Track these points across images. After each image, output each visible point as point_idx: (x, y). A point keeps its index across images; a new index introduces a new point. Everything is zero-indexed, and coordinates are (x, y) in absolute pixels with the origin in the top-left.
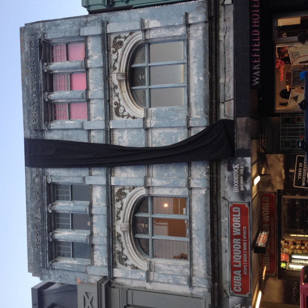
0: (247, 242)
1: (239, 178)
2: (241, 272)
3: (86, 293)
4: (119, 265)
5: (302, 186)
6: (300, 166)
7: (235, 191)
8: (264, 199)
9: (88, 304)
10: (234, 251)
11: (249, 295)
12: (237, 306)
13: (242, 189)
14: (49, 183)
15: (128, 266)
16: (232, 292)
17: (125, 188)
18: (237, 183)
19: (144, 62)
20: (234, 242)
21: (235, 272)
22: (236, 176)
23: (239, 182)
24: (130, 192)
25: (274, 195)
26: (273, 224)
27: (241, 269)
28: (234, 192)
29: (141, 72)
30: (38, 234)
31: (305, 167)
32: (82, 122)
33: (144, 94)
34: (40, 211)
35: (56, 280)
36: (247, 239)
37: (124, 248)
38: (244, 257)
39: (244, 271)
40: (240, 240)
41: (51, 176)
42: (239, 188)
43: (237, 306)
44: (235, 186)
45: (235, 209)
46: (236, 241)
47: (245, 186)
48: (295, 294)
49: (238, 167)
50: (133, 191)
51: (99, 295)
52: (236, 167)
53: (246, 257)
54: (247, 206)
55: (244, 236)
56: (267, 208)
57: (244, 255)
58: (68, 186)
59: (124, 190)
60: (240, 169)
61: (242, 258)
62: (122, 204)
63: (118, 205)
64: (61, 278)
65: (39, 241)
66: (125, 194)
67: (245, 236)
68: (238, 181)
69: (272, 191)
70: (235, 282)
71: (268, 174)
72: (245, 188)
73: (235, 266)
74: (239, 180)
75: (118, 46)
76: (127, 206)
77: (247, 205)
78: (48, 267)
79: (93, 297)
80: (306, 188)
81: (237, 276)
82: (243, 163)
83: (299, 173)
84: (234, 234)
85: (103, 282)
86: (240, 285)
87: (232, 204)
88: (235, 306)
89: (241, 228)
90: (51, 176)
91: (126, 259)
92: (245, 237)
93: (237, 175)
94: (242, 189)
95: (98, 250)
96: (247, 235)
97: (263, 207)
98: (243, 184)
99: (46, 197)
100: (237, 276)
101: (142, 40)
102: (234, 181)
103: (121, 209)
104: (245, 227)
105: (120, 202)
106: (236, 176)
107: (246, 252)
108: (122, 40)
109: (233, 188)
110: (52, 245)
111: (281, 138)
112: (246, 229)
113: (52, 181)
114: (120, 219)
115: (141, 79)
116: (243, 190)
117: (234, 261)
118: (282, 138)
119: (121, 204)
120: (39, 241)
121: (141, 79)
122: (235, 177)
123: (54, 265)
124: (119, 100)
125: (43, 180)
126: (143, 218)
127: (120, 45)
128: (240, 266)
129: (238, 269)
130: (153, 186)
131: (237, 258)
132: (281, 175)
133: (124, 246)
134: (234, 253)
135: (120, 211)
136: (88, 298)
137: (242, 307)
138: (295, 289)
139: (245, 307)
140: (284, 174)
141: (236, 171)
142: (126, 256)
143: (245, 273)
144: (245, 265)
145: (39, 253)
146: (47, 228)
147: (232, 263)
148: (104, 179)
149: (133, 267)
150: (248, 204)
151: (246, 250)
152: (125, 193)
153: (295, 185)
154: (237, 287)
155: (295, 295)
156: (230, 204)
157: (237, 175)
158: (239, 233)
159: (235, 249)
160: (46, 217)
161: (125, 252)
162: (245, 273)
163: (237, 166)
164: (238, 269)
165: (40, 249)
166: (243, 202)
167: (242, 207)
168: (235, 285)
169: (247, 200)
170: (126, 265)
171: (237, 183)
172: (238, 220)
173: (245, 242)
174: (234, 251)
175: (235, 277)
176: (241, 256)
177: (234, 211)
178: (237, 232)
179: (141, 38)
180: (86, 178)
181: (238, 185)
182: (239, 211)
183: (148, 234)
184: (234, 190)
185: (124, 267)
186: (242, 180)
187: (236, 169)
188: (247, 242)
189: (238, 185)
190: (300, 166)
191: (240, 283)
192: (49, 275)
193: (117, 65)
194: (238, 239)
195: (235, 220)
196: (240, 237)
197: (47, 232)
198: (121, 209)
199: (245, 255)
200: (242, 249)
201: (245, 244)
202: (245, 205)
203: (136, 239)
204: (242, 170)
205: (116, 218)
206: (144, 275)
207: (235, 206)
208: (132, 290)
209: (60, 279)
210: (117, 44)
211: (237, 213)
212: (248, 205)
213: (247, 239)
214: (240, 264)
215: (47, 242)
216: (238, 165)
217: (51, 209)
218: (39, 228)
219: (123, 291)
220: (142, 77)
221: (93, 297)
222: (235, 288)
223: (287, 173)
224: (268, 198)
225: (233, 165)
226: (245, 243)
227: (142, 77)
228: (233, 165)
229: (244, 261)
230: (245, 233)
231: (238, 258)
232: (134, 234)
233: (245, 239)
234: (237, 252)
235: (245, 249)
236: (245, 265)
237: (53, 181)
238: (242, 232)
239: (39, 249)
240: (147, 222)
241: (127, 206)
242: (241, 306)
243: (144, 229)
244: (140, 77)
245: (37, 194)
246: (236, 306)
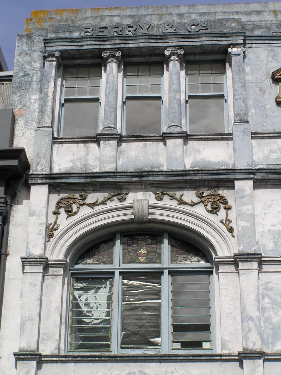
4: (55, 198)
14: (230, 50)
15: (55, 216)
17: (229, 211)
24: (222, 222)
30: (118, 27)
32: (248, 122)
34: (167, 31)
35: (19, 66)
37: (93, 209)
41: (244, 53)
50: (223, 229)
58: (222, 90)
59: (225, 208)
62: (193, 204)
63: (190, 196)
64: (24, 76)
65: (101, 30)
66: (215, 210)
76: (189, 215)
78: (47, 49)
90: (244, 53)
91: (69, 212)
95: (88, 153)
99: (198, 43)
103: (181, 202)
105: (196, 200)
110: (93, 57)
113: (234, 55)
114: (158, 200)
119: (192, 202)
120: (101, 30)
123: (52, 61)
125: (235, 38)
126: (158, 251)
130: (238, 273)
133: (98, 209)
135: (175, 199)
142: (76, 213)
145: (77, 31)
146: (131, 45)
148: (246, 164)
149: (53, 227)
152: (218, 211)
160: (155, 45)
161: (85, 211)
165: (86, 32)
170: (56, 213)
179: (220, 254)
180: (246, 126)
183: (123, 263)
185: (53, 207)
192: (29, 52)
193: (167, 202)
197: (122, 46)
198: (181, 202)
206: (37, 252)
209: (21, 74)
215: (102, 47)
217: (173, 54)
218: (130, 31)
237: (233, 58)
239: (86, 30)
241: (189, 215)
245: (204, 26)
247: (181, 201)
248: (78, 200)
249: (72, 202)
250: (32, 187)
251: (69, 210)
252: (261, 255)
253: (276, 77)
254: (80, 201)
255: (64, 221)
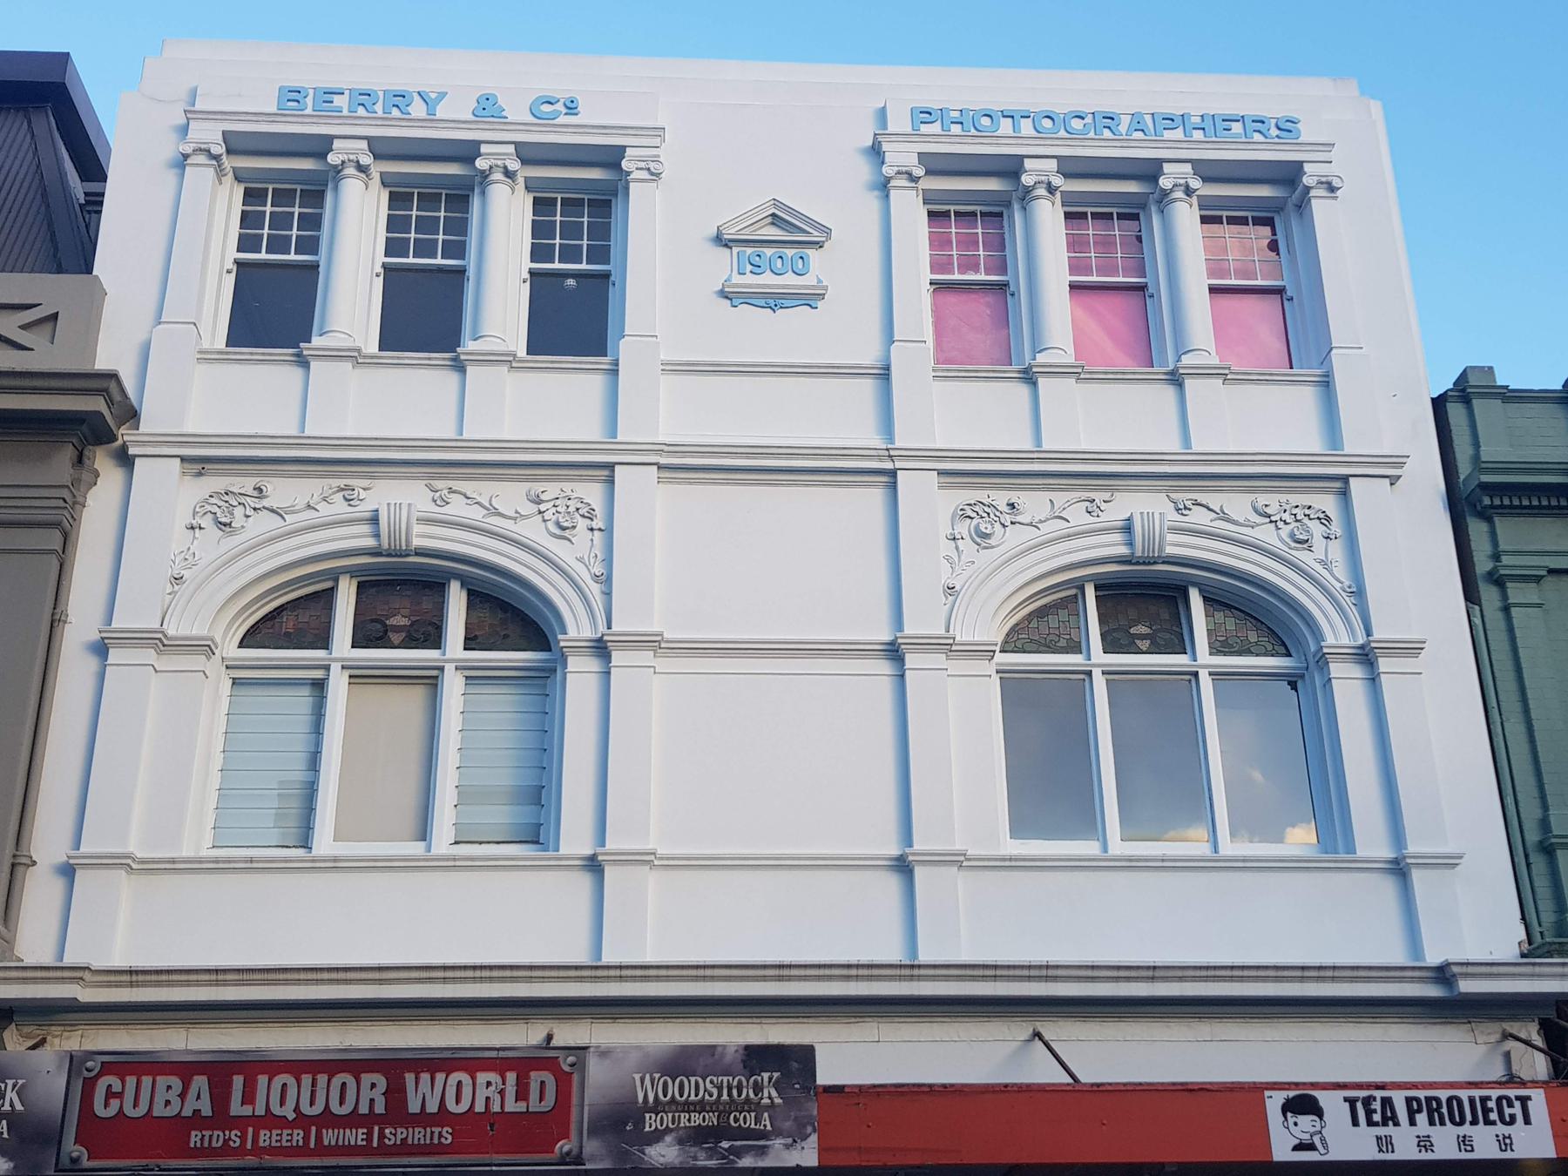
0: (366, 1151)
1: (711, 1104)
2: (204, 1114)
3: (54, 317)
7: (638, 1083)
9: (8, 325)
10: (319, 1077)
11: (75, 1161)
12: (11, 1095)
13: (651, 1122)
16: (89, 1064)
19: (1215, 650)
20: (367, 1079)
21: (200, 1082)
22: (720, 1089)
23: (688, 1107)
27: (221, 1118)
28: (637, 1077)
29: (1168, 636)
33: (1063, 643)
36: (384, 1150)
38: (286, 1132)
39: (207, 1133)
40: (380, 1108)
42: (657, 1107)
43: (11, 1095)
44: (665, 1085)
45: (542, 1083)
46: (372, 1092)
47: (668, 1139)
49: (766, 1101)
51: (54, 383)
53: (285, 1144)
54: (563, 1146)
55: (401, 1133)
57: (296, 1132)
60: (757, 1108)
61: (282, 1122)
62: (518, 517)
67: (399, 1137)
70: (147, 1081)
72: (657, 1136)
73: (238, 1081)
74: (701, 1107)
75: (1291, 527)
77: (566, 1149)
81: (183, 1095)
84: (410, 1078)
85: (110, 402)
86: (129, 1111)
87: (572, 1065)
88: (10, 1083)
89: (443, 1117)
92: (393, 1136)
93: (725, 1097)
94: (651, 1122)
96: (404, 1149)
98: (678, 1128)
100: (183, 1095)
101: (1323, 644)
102: (693, 1079)
104: (450, 1137)
106: (720, 1089)
107: (312, 1145)
109: (657, 1076)
112: (436, 1141)
115: (1132, 631)
116: (647, 1129)
117: (262, 1080)
121: (1132, 631)
122: (712, 1082)
127: (1292, 536)
128: (237, 1108)
129: (220, 1097)
131: (274, 1096)
134: (306, 1080)
136: (25, 327)
137: (4, 1122)
139: (5, 1135)
143: (195, 1138)
144: (243, 1138)
147: (254, 1066)
150: (575, 1152)
151: (326, 1143)
154: (120, 1095)
156: (571, 1059)
157: (725, 1097)
158: (414, 1107)
159: (329, 1081)
162: (195, 1138)
163: (770, 1094)
164: (220, 1097)
166: (585, 1132)
167: (557, 1120)
168: (131, 1081)
169: (591, 1147)
172: (372, 1101)
173: (306, 1138)
174: (319, 1077)
175: (176, 1083)
176: (291, 1116)
177: (535, 1077)
178: (422, 1094)
179: (1330, 639)
182: (534, 1105)
184: (648, 1077)
186: (697, 1119)
187: (758, 1088)
188: (366, 1151)
191: (142, 1110)
194: (383, 1098)
195: (373, 1086)
196: (396, 1110)
199: (298, 1136)
200: (327, 1119)
201: (356, 1137)
202: (566, 1136)
203: (328, 585)
205: (439, 484)
207: (563, 1080)
208: (59, 548)
210: (1297, 521)
211: (522, 1094)
212: (568, 1154)
213: (384, 1150)
214: (247, 1111)
216: (778, 1101)
219: (61, 503)
220: (1143, 637)
221: (32, 350)
222: (113, 1081)
225: (776, 1075)
226: (360, 1137)
227: (1143, 637)
228: (776, 1075)
229: (262, 1132)
230: (418, 1135)
231: (282, 1103)
232: (352, 572)
233: (382, 1136)
234: (313, 1093)
235: (329, 1137)
236: (243, 1138)
238: (423, 1119)
240: (411, 642)
242: (12, 1118)
244: (1142, 629)
246: (14, 1086)
247: (491, 508)
248: (253, 499)
249: (235, 503)
250: (137, 461)
251: (226, 520)
252: (662, 635)
253: (726, 236)
254: (256, 500)
255: (210, 545)
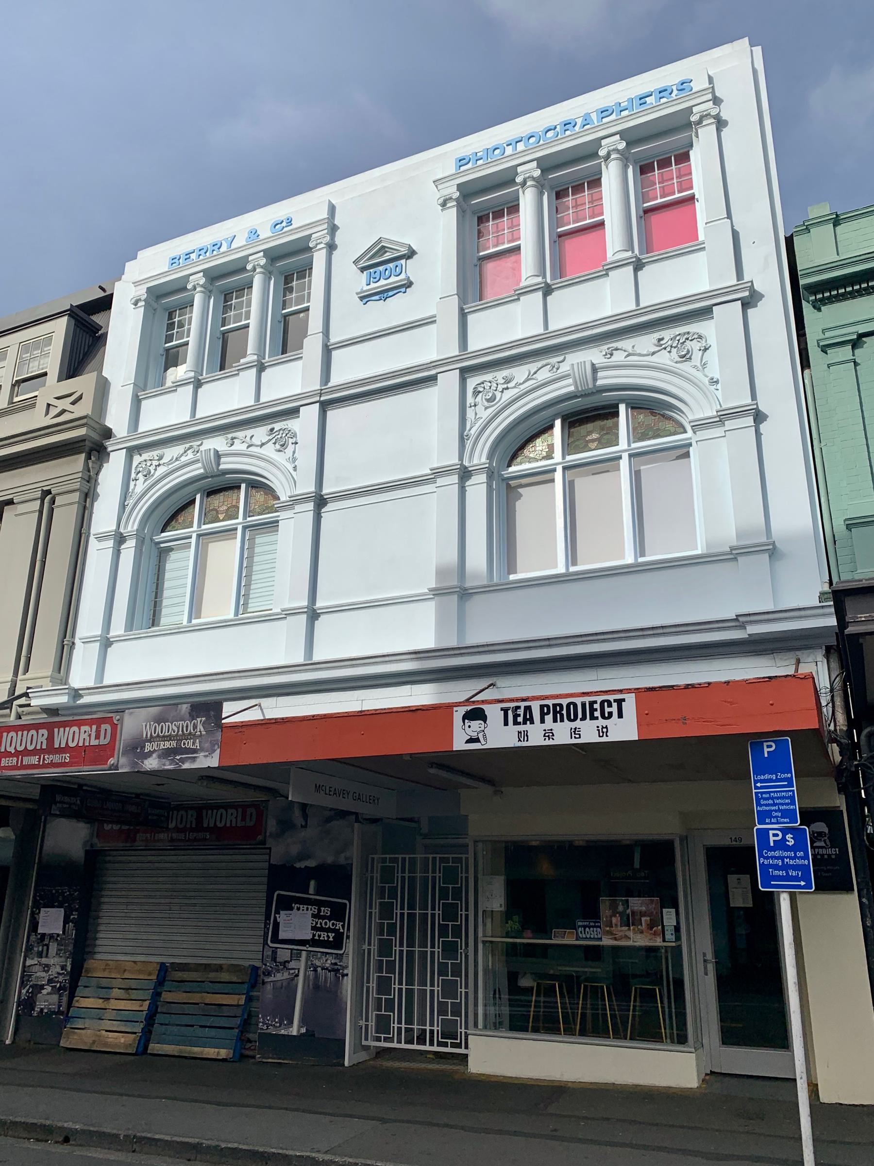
1: (174, 737)
5: (275, 915)
6: (323, 909)
8: (251, 814)
13: (148, 747)
18: (162, 733)
25: (260, 838)
26: (195, 838)
28: (144, 724)
31: (321, 924)
42: (151, 740)
47: (154, 755)
48: (57, 891)
52: (200, 727)
56: (231, 821)
67: (50, 759)
68: (166, 734)
69: (268, 834)
71: (306, 822)
72: (150, 754)
74: (169, 738)
79: (57, 407)
80: (271, 925)
82: (207, 745)
83: (306, 906)
89: (67, 749)
92: (49, 758)
93: (180, 732)
97: (234, 811)
108: (697, 356)
109: (152, 723)
111: (433, 858)
118: (404, 859)
122: (175, 725)
124: (517, 385)
132: (301, 857)
138: (66, 892)
140: (306, 866)
141: (191, 728)
153: (278, 895)
155: (54, 891)
156: (118, 717)
157: (180, 732)
171: (162, 733)
176: (13, 751)
181: (158, 736)
186: (167, 745)
187: (195, 727)
189: (158, 736)
190: (323, 909)
193: (618, 357)
200: (26, 752)
204: (189, 744)
205: (230, 436)
207: (114, 727)
220: (593, 441)
223: (310, 873)
224: (252, 824)
227: (593, 441)
228: (204, 719)
230: (57, 758)
235: (27, 760)
238: (60, 750)
243: (216, 510)
